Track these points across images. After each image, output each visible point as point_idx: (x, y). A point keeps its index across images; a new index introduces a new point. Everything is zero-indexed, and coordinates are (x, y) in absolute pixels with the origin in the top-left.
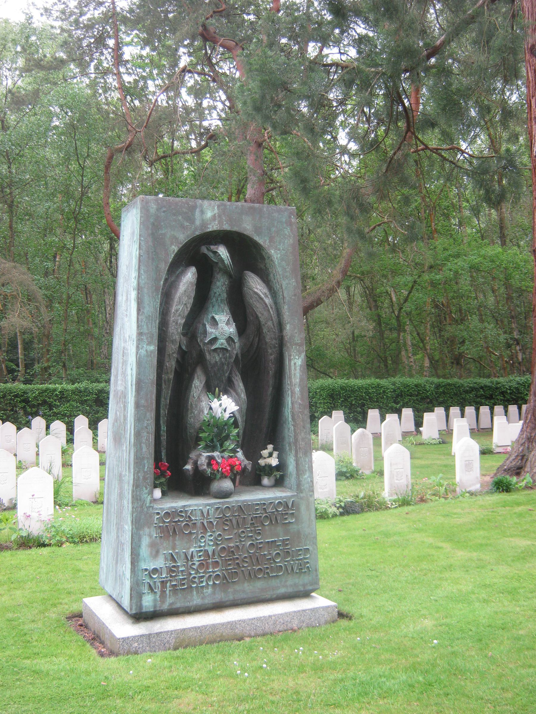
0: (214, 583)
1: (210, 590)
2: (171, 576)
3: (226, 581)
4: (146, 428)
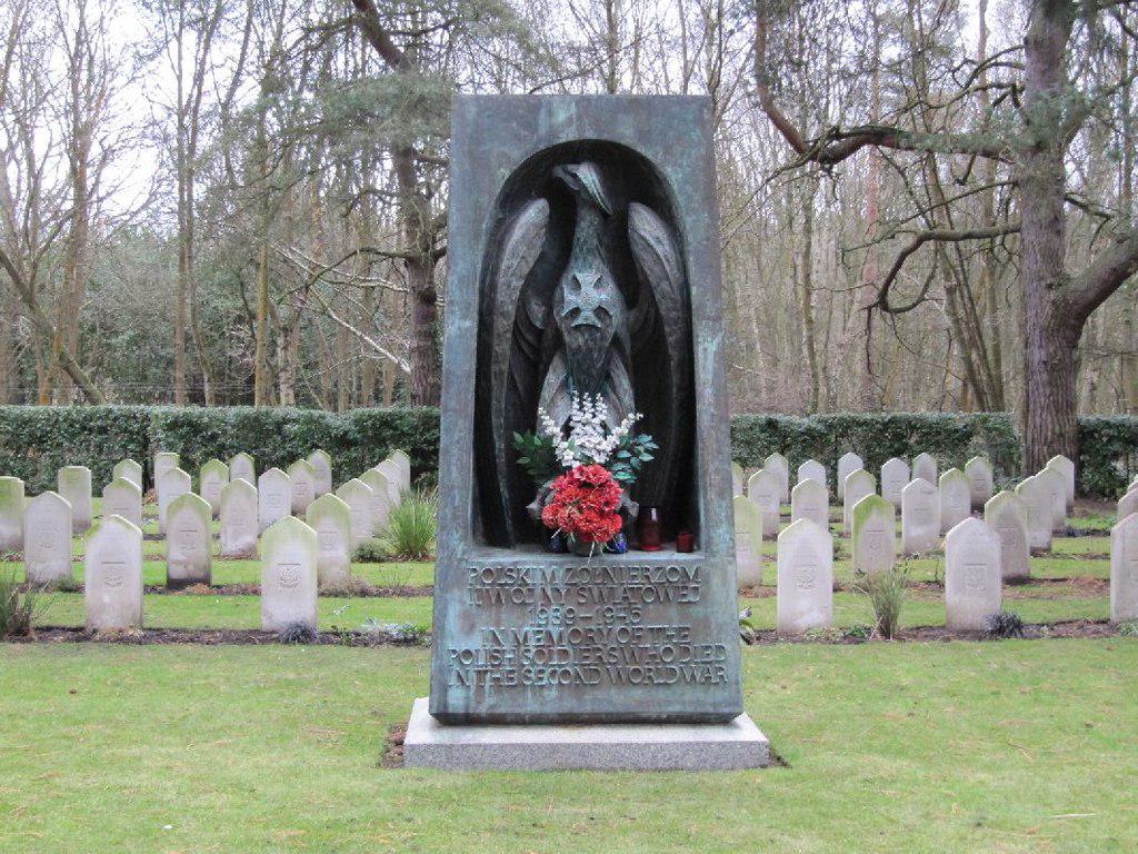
0: (560, 683)
1: (554, 693)
2: (493, 666)
3: (578, 686)
4: (458, 442)
